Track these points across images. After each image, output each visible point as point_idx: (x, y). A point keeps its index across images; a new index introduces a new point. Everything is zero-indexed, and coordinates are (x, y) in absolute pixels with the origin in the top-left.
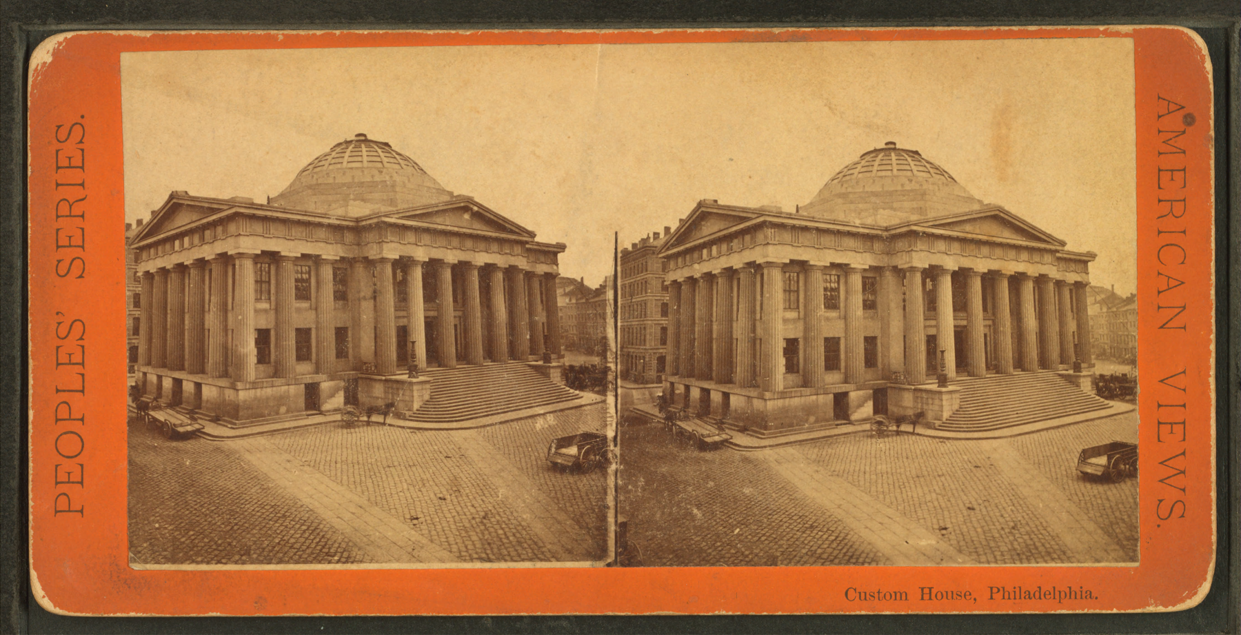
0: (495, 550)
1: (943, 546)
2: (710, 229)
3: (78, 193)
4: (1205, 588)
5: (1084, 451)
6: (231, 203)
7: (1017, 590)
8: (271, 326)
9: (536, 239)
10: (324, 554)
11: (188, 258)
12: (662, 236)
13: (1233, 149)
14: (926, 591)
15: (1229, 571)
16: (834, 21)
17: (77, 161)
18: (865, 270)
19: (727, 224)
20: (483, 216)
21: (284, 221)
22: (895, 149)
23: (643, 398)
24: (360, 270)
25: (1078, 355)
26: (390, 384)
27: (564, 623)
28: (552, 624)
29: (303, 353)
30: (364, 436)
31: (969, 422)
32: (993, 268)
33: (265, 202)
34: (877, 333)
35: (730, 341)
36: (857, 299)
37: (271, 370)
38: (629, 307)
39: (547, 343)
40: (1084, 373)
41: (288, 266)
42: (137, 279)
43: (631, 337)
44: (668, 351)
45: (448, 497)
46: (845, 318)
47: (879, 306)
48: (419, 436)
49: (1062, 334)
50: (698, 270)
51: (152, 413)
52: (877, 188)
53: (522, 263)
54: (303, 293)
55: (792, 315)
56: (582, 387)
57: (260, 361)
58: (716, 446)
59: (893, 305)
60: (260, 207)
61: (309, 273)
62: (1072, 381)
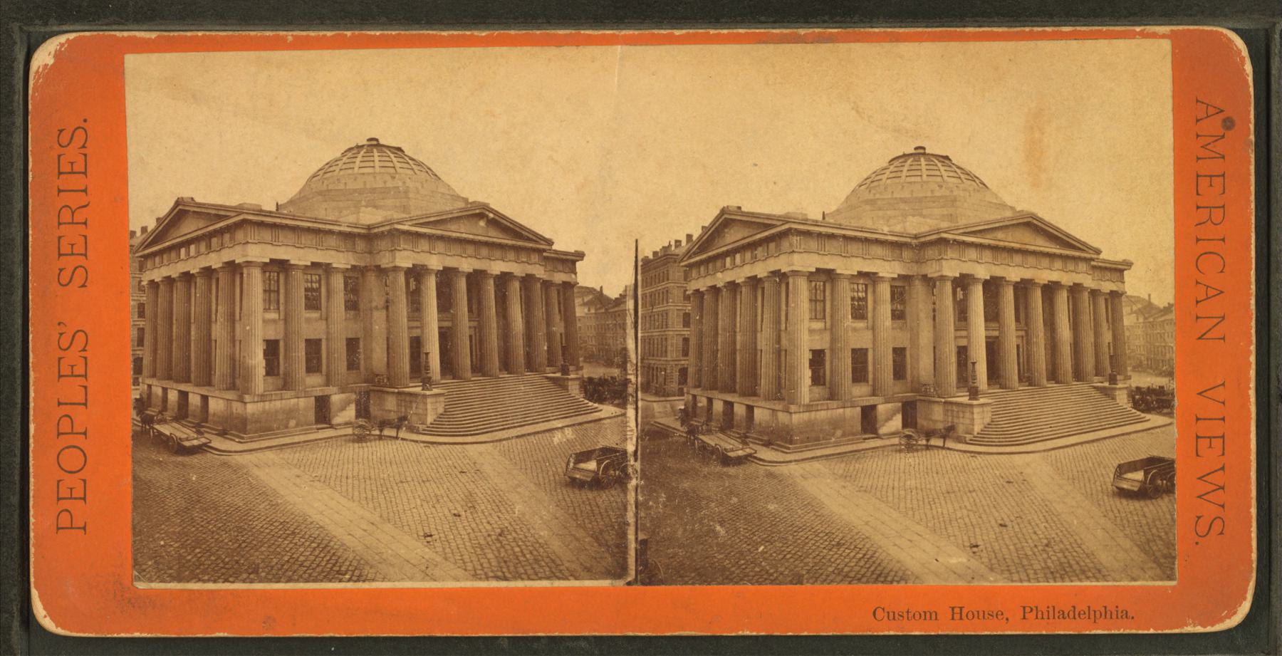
0: (512, 569)
1: (974, 564)
2: (733, 237)
3: (80, 199)
4: (1245, 608)
5: (1120, 466)
6: (239, 210)
7: (1051, 610)
8: (280, 336)
9: (554, 247)
10: (335, 573)
11: (194, 267)
12: (684, 243)
13: (1274, 154)
14: (957, 610)
15: (1270, 590)
16: (861, 21)
18: (893, 279)
20: (499, 223)
22: (924, 154)
23: (665, 412)
24: (372, 279)
25: (1113, 367)
27: (583, 644)
28: (570, 644)
29: (313, 365)
30: (377, 450)
31: (1002, 436)
33: (274, 209)
34: (906, 344)
35: (754, 352)
36: (886, 309)
38: (650, 317)
39: (566, 354)
40: (572, 376)
41: (298, 275)
42: (141, 289)
43: (652, 348)
44: (690, 362)
46: (873, 329)
47: (908, 317)
48: (432, 450)
49: (1097, 345)
50: (721, 279)
51: (157, 427)
52: (906, 195)
53: (539, 272)
54: (313, 302)
55: (818, 325)
56: (601, 400)
58: (739, 461)
59: (922, 315)
60: (269, 214)
61: (319, 282)
62: (1108, 393)
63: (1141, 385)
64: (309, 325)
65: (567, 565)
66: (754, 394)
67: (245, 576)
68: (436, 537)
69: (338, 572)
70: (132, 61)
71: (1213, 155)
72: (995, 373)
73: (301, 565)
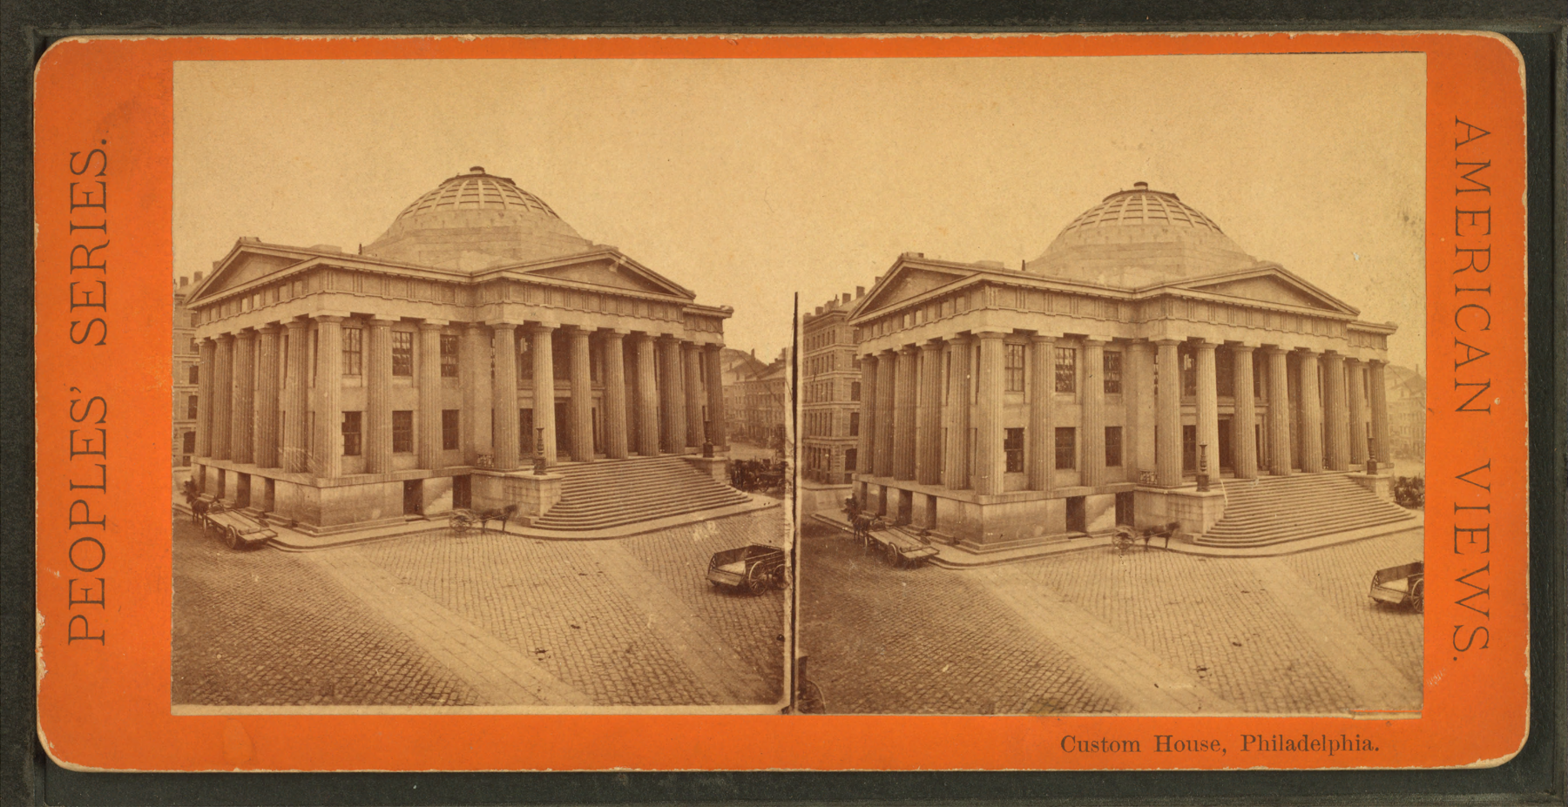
1: (1202, 691)
2: (914, 290)
3: (95, 238)
5: (717, 556)
6: (314, 253)
8: (363, 408)
9: (696, 301)
10: (427, 696)
12: (854, 297)
14: (1163, 740)
17: (96, 198)
18: (445, 327)
19: (268, 269)
20: (631, 272)
21: (1046, 292)
22: (484, 176)
23: (829, 504)
24: (474, 337)
25: (709, 434)
26: (1174, 500)
28: (705, 782)
30: (477, 547)
31: (1232, 536)
32: (1302, 345)
34: (459, 405)
35: (937, 433)
36: (1098, 378)
37: (361, 462)
38: (811, 389)
39: (709, 434)
40: (716, 458)
41: (384, 334)
42: (195, 348)
43: (817, 423)
44: (860, 443)
45: (583, 626)
46: (1082, 404)
47: (461, 374)
49: (689, 407)
51: (211, 516)
52: (1124, 241)
53: (678, 331)
54: (402, 366)
55: (1015, 399)
56: (752, 488)
57: (1009, 469)
58: (920, 563)
59: (478, 370)
60: (351, 258)
61: (1074, 358)
62: (1364, 484)
63: (1406, 475)
64: (398, 394)
65: (709, 687)
66: (937, 481)
67: (317, 698)
68: (550, 653)
69: (430, 695)
70: (183, 71)
71: (1474, 186)
72: (1228, 460)
73: (386, 686)
